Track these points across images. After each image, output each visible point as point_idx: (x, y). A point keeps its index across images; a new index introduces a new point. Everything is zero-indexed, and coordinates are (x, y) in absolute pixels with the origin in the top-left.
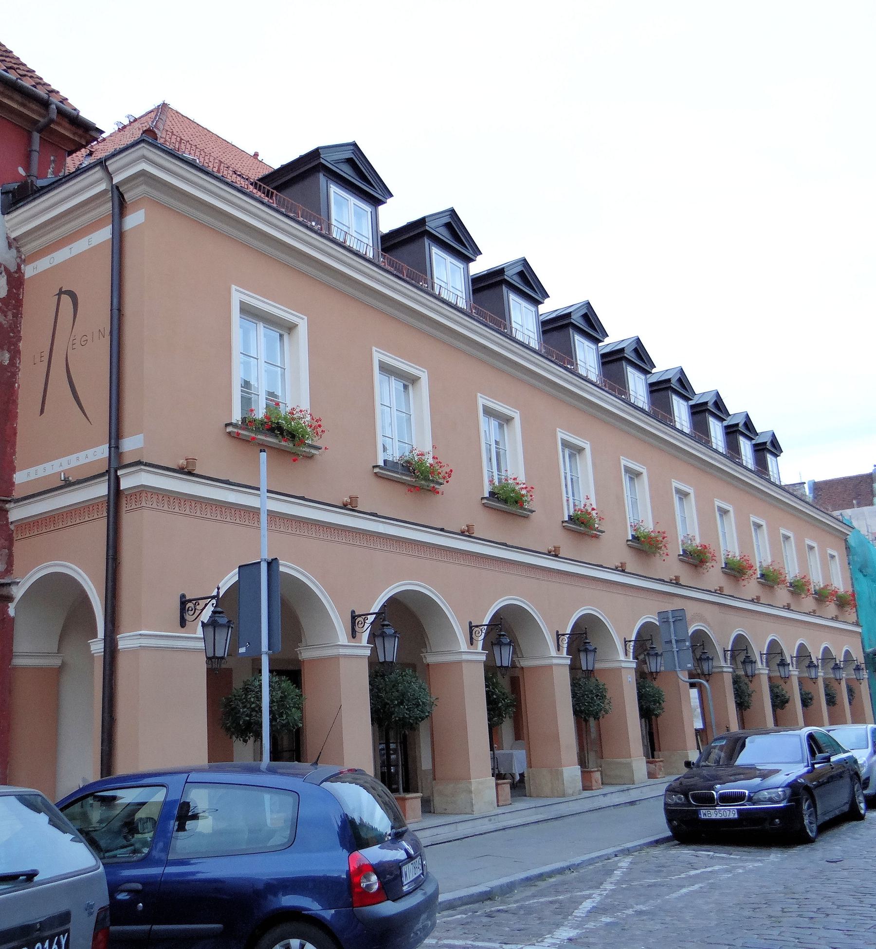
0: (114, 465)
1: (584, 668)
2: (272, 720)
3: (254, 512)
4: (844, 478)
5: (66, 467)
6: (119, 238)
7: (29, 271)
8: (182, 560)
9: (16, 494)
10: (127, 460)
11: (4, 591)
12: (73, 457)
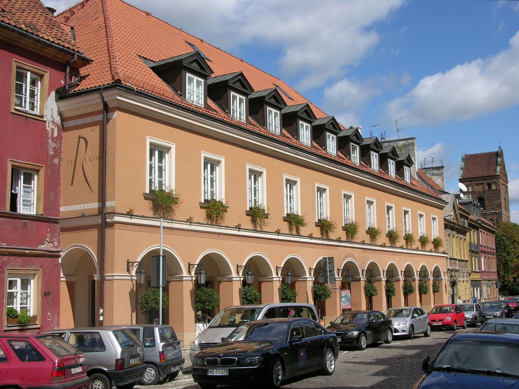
1: (253, 276)
2: (163, 306)
3: (159, 227)
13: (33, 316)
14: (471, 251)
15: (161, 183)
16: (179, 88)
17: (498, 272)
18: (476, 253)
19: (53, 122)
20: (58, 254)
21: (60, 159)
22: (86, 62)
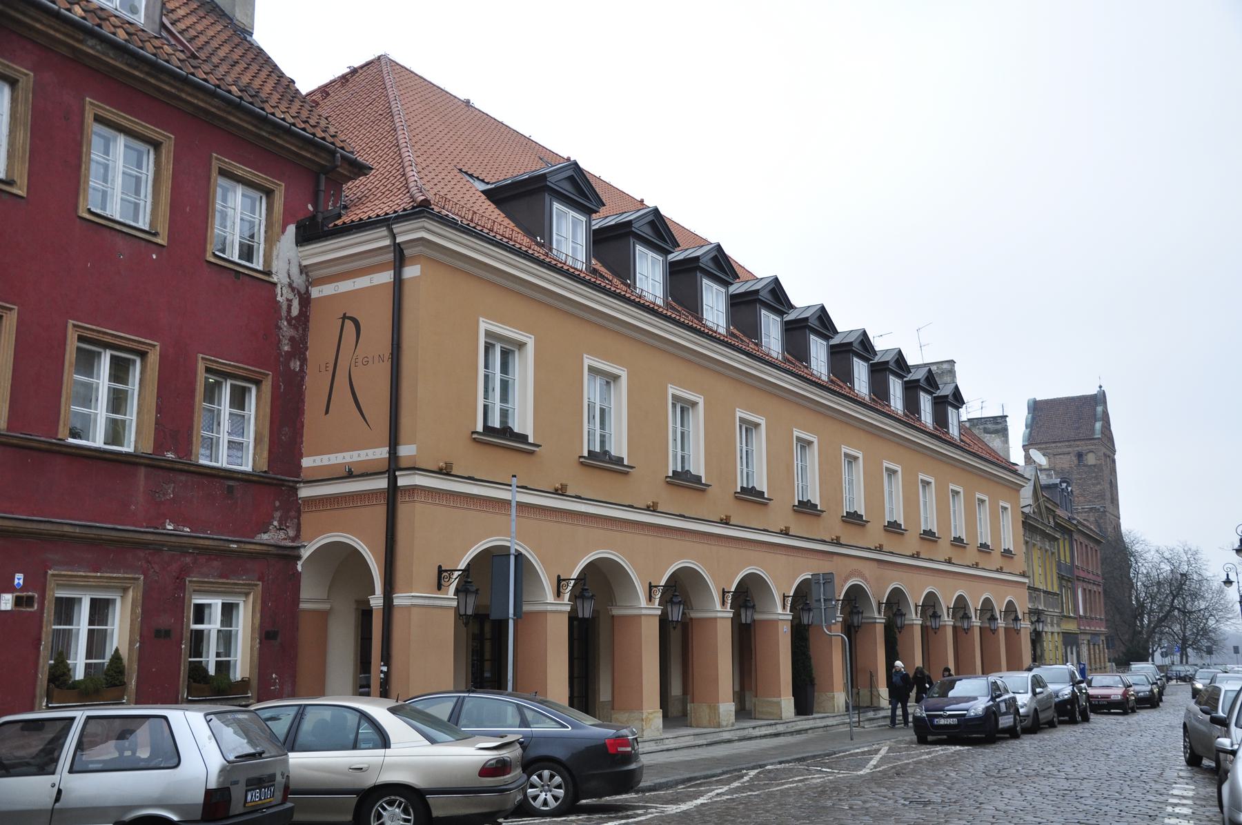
4: (1067, 399)
6: (398, 283)
7: (315, 293)
8: (444, 541)
10: (403, 464)
13: (243, 680)
14: (1061, 578)
15: (504, 414)
16: (539, 229)
18: (1068, 580)
19: (290, 285)
20: (295, 553)
21: (304, 361)
22: (360, 169)
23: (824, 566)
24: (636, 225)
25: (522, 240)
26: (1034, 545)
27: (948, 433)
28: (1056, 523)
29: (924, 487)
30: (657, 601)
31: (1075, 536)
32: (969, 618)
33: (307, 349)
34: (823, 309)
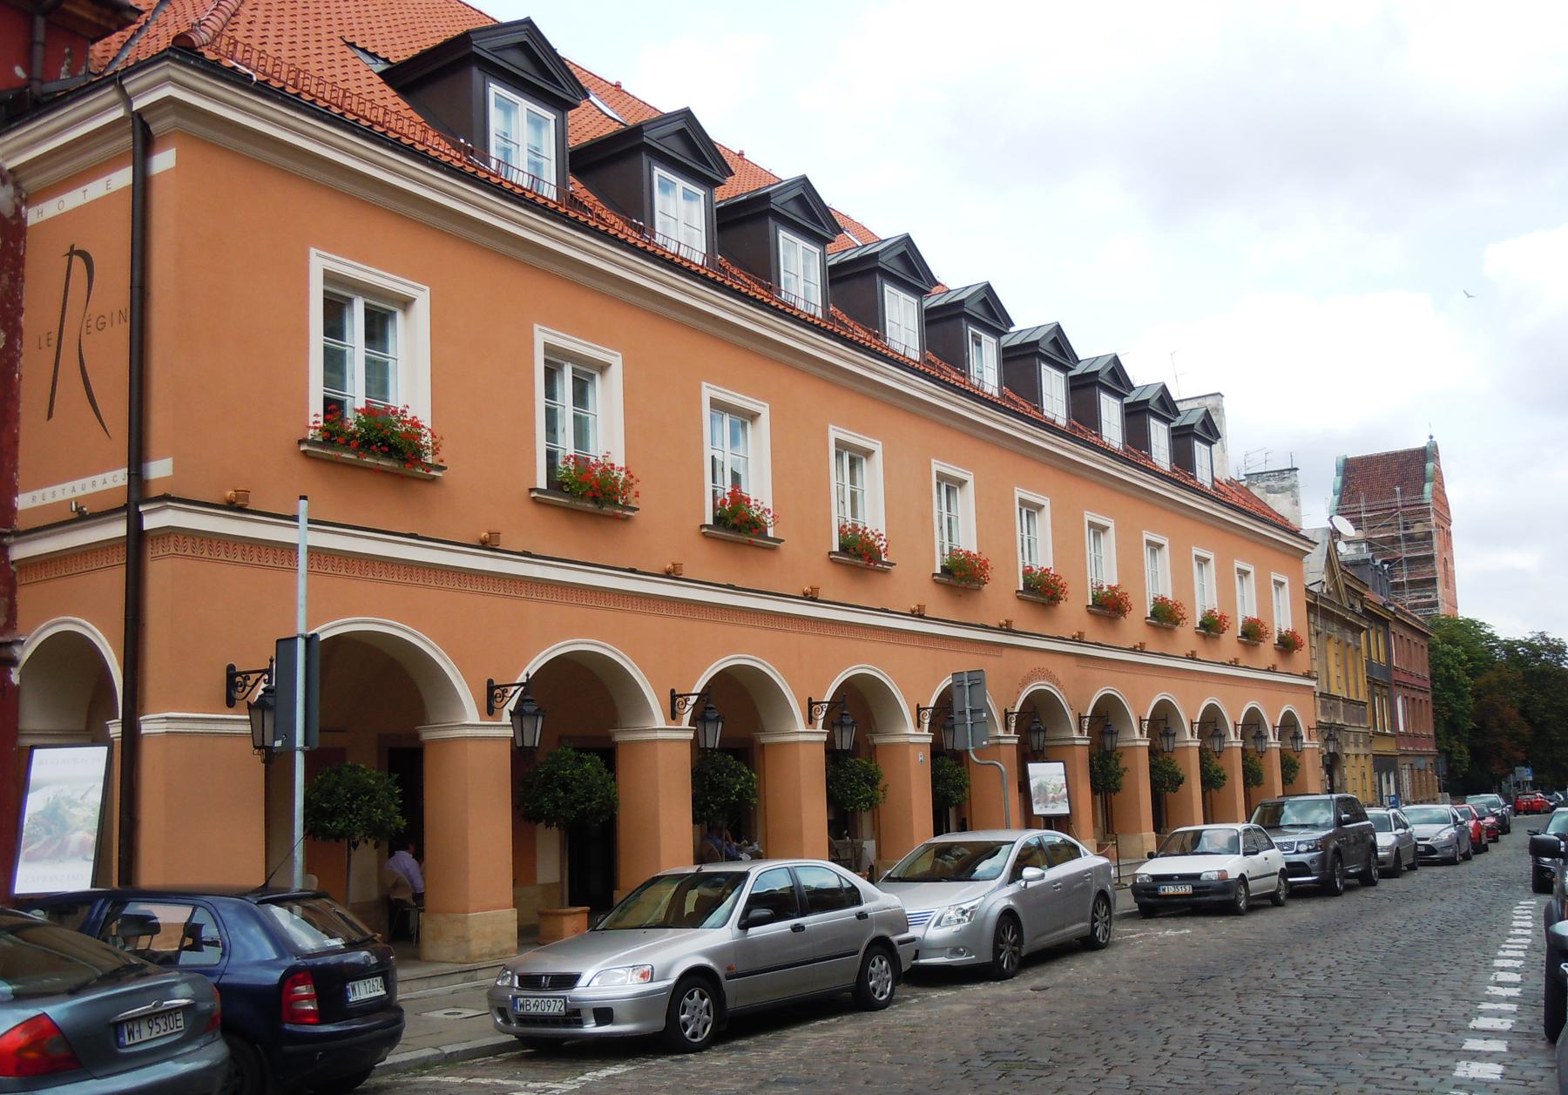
0: (135, 497)
5: (79, 493)
6: (142, 185)
7: (33, 216)
9: (20, 524)
11: (4, 653)
12: (88, 481)
14: (1372, 682)
17: (1436, 735)
23: (967, 662)
24: (883, 259)
25: (436, 144)
26: (1329, 637)
27: (1194, 477)
28: (1365, 610)
29: (1200, 566)
30: (820, 723)
31: (1393, 627)
32: (1222, 737)
33: (20, 311)
34: (1058, 329)
